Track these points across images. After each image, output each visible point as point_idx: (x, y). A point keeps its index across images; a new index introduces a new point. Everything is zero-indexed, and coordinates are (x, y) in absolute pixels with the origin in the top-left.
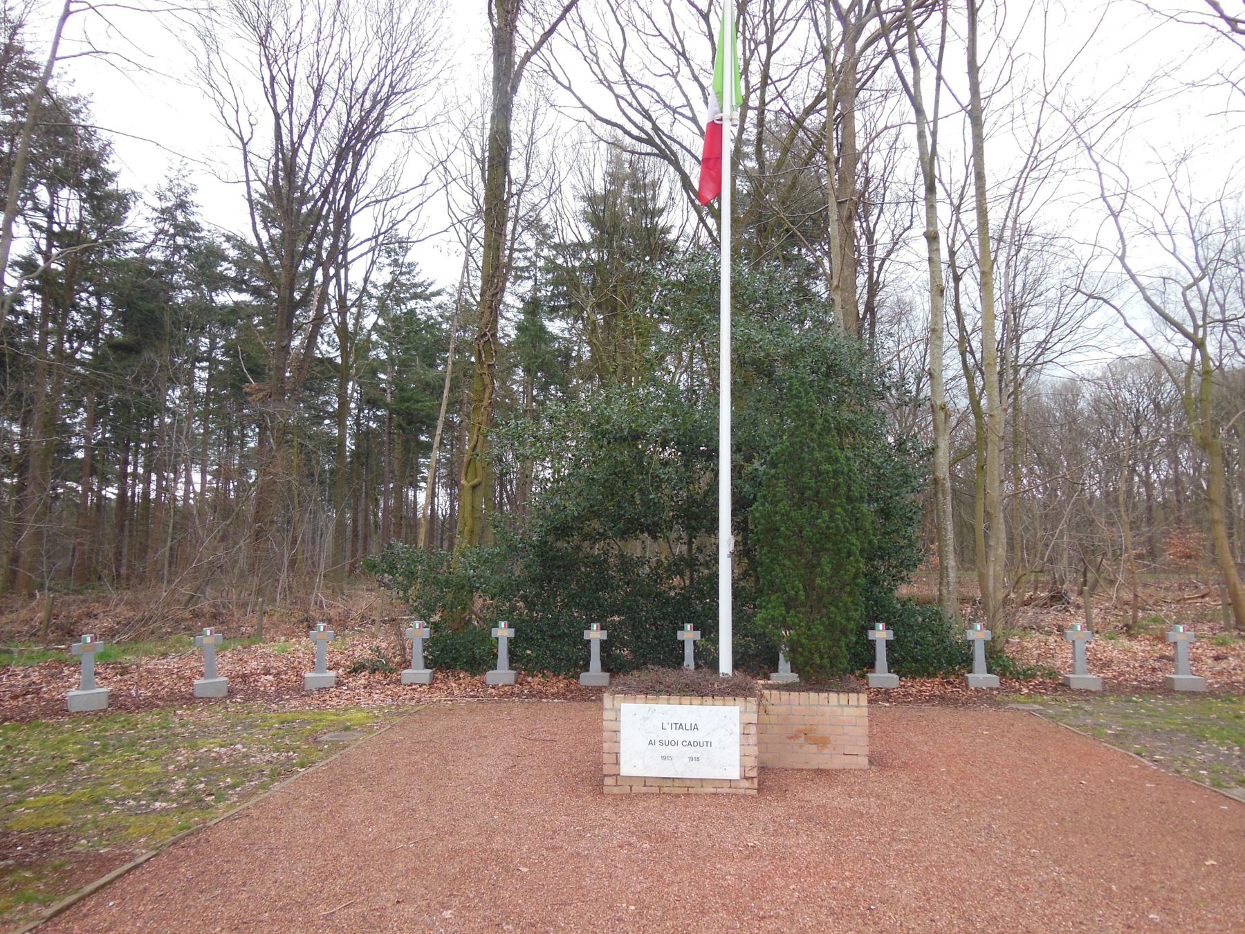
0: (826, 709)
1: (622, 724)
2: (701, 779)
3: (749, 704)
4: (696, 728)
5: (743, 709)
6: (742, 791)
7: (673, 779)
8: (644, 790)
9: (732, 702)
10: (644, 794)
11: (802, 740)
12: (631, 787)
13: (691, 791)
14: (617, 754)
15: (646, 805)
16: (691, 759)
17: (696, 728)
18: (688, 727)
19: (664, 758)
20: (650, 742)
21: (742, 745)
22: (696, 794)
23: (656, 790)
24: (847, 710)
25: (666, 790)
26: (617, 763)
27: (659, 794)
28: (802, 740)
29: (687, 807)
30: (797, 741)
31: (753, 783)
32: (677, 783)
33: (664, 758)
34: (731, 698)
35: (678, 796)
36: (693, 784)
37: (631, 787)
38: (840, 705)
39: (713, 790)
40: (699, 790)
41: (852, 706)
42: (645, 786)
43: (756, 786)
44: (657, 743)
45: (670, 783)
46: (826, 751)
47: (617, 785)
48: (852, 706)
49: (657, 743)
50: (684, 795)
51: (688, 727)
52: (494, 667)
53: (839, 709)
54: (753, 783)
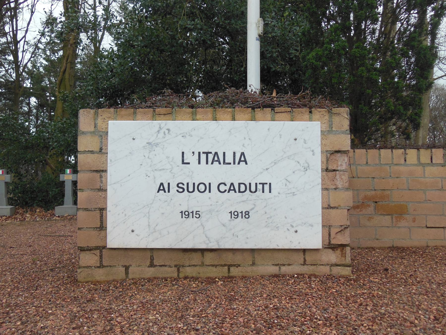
0: (402, 168)
1: (110, 156)
2: (252, 250)
3: (336, 119)
4: (243, 159)
5: (326, 127)
6: (325, 270)
7: (203, 251)
8: (150, 272)
9: (307, 116)
10: (150, 280)
11: (371, 210)
12: (127, 268)
13: (234, 271)
14: (102, 210)
15: (149, 297)
16: (234, 215)
17: (243, 159)
18: (229, 159)
19: (186, 214)
20: (161, 188)
21: (325, 189)
22: (243, 277)
23: (171, 272)
24: (429, 170)
25: (189, 271)
26: (102, 227)
27: (177, 279)
28: (371, 210)
29: (231, 300)
30: (364, 211)
31: (343, 255)
32: (209, 258)
33: (186, 214)
34: (305, 110)
35: (211, 281)
36: (238, 259)
37: (127, 268)
38: (420, 164)
39: (274, 270)
40: (248, 270)
41: (438, 165)
42: (152, 265)
43: (348, 260)
44: (174, 188)
45: (196, 259)
46: (403, 223)
47: (101, 266)
48: (438, 165)
49: (174, 188)
50: (223, 279)
51: (229, 159)
52: (62, 203)
53: (420, 169)
54: (343, 255)
